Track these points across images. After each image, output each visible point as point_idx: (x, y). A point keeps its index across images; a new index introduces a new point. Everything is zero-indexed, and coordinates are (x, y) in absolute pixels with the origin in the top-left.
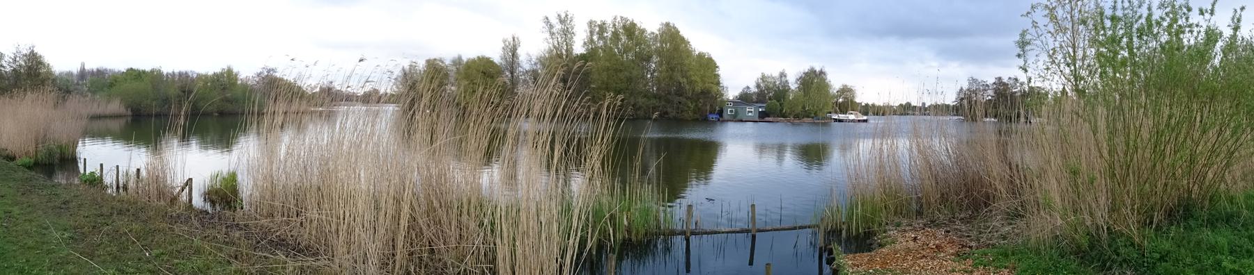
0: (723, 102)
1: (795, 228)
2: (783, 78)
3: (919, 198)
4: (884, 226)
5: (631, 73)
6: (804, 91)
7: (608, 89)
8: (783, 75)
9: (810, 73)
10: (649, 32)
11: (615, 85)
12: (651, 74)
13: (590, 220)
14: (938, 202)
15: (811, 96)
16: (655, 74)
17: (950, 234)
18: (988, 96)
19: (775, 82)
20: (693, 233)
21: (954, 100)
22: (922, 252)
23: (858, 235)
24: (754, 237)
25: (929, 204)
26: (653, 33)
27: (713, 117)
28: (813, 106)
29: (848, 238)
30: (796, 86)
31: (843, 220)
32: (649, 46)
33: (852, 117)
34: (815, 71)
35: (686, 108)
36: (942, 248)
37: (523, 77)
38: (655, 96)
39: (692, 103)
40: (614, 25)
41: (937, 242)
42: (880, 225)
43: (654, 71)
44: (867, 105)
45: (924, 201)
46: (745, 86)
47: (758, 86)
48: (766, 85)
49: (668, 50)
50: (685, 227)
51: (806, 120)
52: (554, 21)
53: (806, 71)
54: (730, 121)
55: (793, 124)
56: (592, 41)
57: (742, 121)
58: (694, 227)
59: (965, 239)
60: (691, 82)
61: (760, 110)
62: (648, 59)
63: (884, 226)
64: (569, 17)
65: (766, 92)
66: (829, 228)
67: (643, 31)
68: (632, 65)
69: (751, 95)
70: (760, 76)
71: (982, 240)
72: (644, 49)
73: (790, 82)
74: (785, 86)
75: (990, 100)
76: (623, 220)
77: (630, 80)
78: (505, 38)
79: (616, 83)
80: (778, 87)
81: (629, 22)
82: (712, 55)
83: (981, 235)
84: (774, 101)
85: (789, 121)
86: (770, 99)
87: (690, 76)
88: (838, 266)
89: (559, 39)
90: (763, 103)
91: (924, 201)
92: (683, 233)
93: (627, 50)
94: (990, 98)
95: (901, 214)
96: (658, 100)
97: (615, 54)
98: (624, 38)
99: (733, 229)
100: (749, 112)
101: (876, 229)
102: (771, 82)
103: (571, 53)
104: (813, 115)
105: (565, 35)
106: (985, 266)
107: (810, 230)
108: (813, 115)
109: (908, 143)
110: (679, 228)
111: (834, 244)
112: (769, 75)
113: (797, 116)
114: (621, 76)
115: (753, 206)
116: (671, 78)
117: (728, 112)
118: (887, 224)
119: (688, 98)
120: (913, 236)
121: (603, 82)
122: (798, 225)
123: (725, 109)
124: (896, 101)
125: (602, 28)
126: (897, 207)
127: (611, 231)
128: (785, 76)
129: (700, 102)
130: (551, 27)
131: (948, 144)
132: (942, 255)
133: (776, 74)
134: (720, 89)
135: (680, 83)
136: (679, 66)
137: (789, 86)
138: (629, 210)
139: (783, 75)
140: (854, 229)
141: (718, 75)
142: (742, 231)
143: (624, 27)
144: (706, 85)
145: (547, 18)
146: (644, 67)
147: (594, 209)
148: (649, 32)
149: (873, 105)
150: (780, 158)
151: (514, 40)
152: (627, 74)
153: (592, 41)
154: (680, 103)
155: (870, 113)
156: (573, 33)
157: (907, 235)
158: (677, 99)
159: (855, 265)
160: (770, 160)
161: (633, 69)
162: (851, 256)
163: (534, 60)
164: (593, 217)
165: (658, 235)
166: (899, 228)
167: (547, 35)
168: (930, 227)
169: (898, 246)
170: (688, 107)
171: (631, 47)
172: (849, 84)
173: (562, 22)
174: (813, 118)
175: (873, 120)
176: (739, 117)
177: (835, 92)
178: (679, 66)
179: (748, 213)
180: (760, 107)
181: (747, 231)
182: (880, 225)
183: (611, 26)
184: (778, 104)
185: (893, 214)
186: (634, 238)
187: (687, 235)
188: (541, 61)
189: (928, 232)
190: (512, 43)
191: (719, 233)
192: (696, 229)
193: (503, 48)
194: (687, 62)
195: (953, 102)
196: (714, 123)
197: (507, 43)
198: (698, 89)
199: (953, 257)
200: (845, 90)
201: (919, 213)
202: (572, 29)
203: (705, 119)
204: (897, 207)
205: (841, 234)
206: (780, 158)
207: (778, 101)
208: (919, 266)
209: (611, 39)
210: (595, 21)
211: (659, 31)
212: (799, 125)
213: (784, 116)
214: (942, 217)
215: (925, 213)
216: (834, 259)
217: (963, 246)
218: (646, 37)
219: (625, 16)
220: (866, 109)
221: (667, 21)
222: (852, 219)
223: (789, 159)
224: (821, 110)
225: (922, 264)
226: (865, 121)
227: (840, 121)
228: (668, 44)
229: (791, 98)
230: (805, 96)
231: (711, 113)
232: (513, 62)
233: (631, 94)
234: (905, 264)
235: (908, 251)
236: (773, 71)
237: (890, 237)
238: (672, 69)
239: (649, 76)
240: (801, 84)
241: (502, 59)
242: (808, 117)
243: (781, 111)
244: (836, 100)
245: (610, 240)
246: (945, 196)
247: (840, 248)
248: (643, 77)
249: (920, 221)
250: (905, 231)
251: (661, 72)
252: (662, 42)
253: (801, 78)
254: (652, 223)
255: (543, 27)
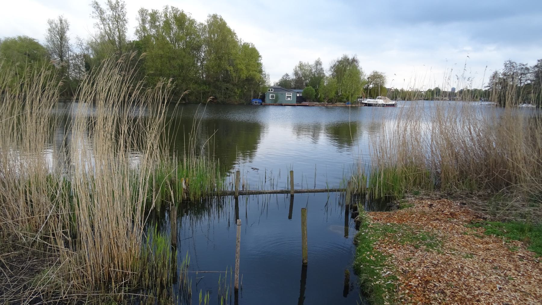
0: (265, 88)
1: (326, 191)
2: (319, 66)
3: (437, 172)
4: (403, 194)
5: (182, 61)
6: (338, 78)
7: (161, 75)
8: (318, 63)
9: (343, 61)
10: (198, 23)
11: (168, 72)
12: (201, 62)
13: (154, 185)
14: (457, 178)
15: (344, 82)
16: (205, 62)
17: (466, 206)
18: (526, 80)
19: (311, 70)
20: (241, 193)
21: (487, 85)
22: (436, 216)
23: (380, 198)
24: (292, 196)
25: (447, 179)
26: (202, 24)
27: (256, 101)
28: (346, 92)
29: (372, 200)
30: (330, 73)
31: (367, 187)
32: (198, 36)
33: (381, 101)
34: (348, 59)
35: (233, 94)
36: (456, 215)
37: (74, 61)
38: (204, 83)
39: (238, 89)
40: (166, 15)
41: (452, 210)
42: (400, 192)
43: (204, 59)
44: (396, 90)
45: (443, 175)
46: (284, 74)
47: (296, 74)
48: (303, 73)
49: (216, 41)
50: (234, 189)
51: (338, 104)
52: (104, 6)
53: (340, 59)
54: (272, 105)
55: (327, 107)
56: (144, 29)
57: (281, 105)
58: (241, 189)
59: (480, 212)
60: (237, 70)
61: (298, 95)
62: (198, 48)
63: (403, 194)
64: (120, 4)
65: (303, 78)
66: (355, 192)
67: (192, 22)
68: (184, 53)
69: (290, 82)
70: (298, 64)
71: (498, 215)
72: (194, 39)
73: (324, 69)
74: (320, 73)
75: (528, 84)
76: (181, 184)
77: (182, 67)
78: (51, 19)
79: (170, 70)
80: (314, 75)
81: (179, 13)
82: (255, 46)
83: (498, 211)
84: (310, 87)
85: (323, 105)
86: (307, 85)
87: (237, 64)
88: (361, 218)
89: (111, 25)
90: (300, 89)
91: (443, 175)
92: (232, 193)
93: (178, 39)
94: (529, 82)
95: (420, 185)
96: (208, 86)
97: (168, 43)
98: (175, 27)
99: (275, 189)
100: (288, 97)
101: (396, 194)
102: (307, 70)
103: (124, 40)
104: (345, 100)
105: (117, 22)
106: (498, 235)
107: (339, 193)
108: (345, 100)
109: (431, 125)
110: (230, 190)
111: (358, 203)
112: (306, 63)
113: (330, 101)
114: (175, 63)
115: (292, 172)
116: (219, 66)
117: (270, 97)
118: (406, 192)
119: (234, 85)
120: (429, 203)
121: (157, 70)
122: (330, 188)
123: (267, 94)
124: (424, 85)
125: (154, 16)
126: (416, 178)
127: (172, 193)
128: (320, 64)
129: (245, 89)
130: (102, 12)
131: (472, 128)
132: (455, 220)
133: (312, 63)
134: (263, 76)
135: (227, 71)
136: (226, 56)
137: (323, 74)
138: (187, 176)
139: (318, 63)
140: (377, 193)
141: (261, 64)
142: (282, 192)
143: (175, 17)
144: (251, 72)
145: (97, 3)
146: (194, 56)
147: (157, 176)
148: (198, 23)
149: (402, 91)
150: (315, 137)
151: (61, 22)
152: (179, 62)
153: (144, 29)
154: (227, 89)
155: (398, 99)
156: (125, 20)
157: (424, 201)
158: (224, 86)
159: (375, 219)
160: (306, 140)
161: (184, 57)
162: (373, 213)
163: (85, 45)
164: (156, 182)
165: (212, 195)
166: (417, 197)
167: (98, 21)
168: (447, 198)
169: (414, 210)
170: (235, 93)
171: (182, 37)
172: (380, 71)
173: (113, 8)
174: (345, 102)
175: (400, 104)
176: (279, 102)
177: (366, 78)
178: (226, 56)
179: (288, 178)
180: (298, 93)
181: (287, 192)
182: (400, 192)
183: (163, 16)
184: (314, 90)
185: (412, 184)
186: (192, 198)
187: (236, 195)
188: (92, 47)
189: (444, 201)
190: (59, 25)
191: (264, 193)
192: (243, 190)
193: (49, 30)
194: (233, 51)
195: (485, 87)
196: (256, 107)
197: (54, 25)
198: (243, 76)
199: (466, 224)
200: (377, 77)
201: (437, 187)
202: (124, 16)
203: (249, 104)
204: (416, 178)
205: (365, 197)
206: (315, 137)
207: (314, 87)
208: (432, 225)
209: (163, 28)
210: (146, 10)
211: (208, 22)
212: (332, 108)
213: (319, 100)
214: (459, 191)
215: (443, 186)
216: (358, 214)
217: (477, 217)
218: (195, 27)
219: (176, 6)
220: (396, 95)
221: (215, 13)
222: (375, 186)
223: (323, 138)
224: (352, 95)
225: (434, 224)
226: (393, 105)
227: (370, 105)
228: (216, 35)
229: (325, 84)
230: (338, 83)
231: (254, 98)
232: (61, 46)
233: (183, 80)
234: (420, 223)
235: (424, 214)
236: (310, 60)
237: (407, 201)
238: (220, 59)
239: (199, 64)
240: (335, 71)
241: (48, 41)
242: (341, 101)
243: (316, 96)
244: (366, 85)
245: (171, 200)
246: (465, 173)
247: (363, 207)
248: (194, 65)
249: (438, 193)
250: (422, 199)
251: (210, 60)
252: (210, 32)
253: (334, 65)
254: (207, 186)
255: (93, 12)
